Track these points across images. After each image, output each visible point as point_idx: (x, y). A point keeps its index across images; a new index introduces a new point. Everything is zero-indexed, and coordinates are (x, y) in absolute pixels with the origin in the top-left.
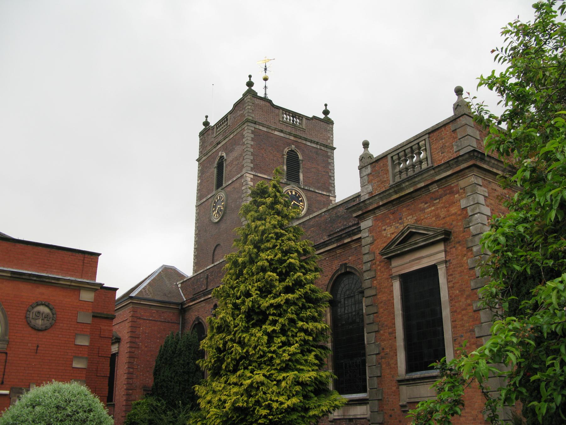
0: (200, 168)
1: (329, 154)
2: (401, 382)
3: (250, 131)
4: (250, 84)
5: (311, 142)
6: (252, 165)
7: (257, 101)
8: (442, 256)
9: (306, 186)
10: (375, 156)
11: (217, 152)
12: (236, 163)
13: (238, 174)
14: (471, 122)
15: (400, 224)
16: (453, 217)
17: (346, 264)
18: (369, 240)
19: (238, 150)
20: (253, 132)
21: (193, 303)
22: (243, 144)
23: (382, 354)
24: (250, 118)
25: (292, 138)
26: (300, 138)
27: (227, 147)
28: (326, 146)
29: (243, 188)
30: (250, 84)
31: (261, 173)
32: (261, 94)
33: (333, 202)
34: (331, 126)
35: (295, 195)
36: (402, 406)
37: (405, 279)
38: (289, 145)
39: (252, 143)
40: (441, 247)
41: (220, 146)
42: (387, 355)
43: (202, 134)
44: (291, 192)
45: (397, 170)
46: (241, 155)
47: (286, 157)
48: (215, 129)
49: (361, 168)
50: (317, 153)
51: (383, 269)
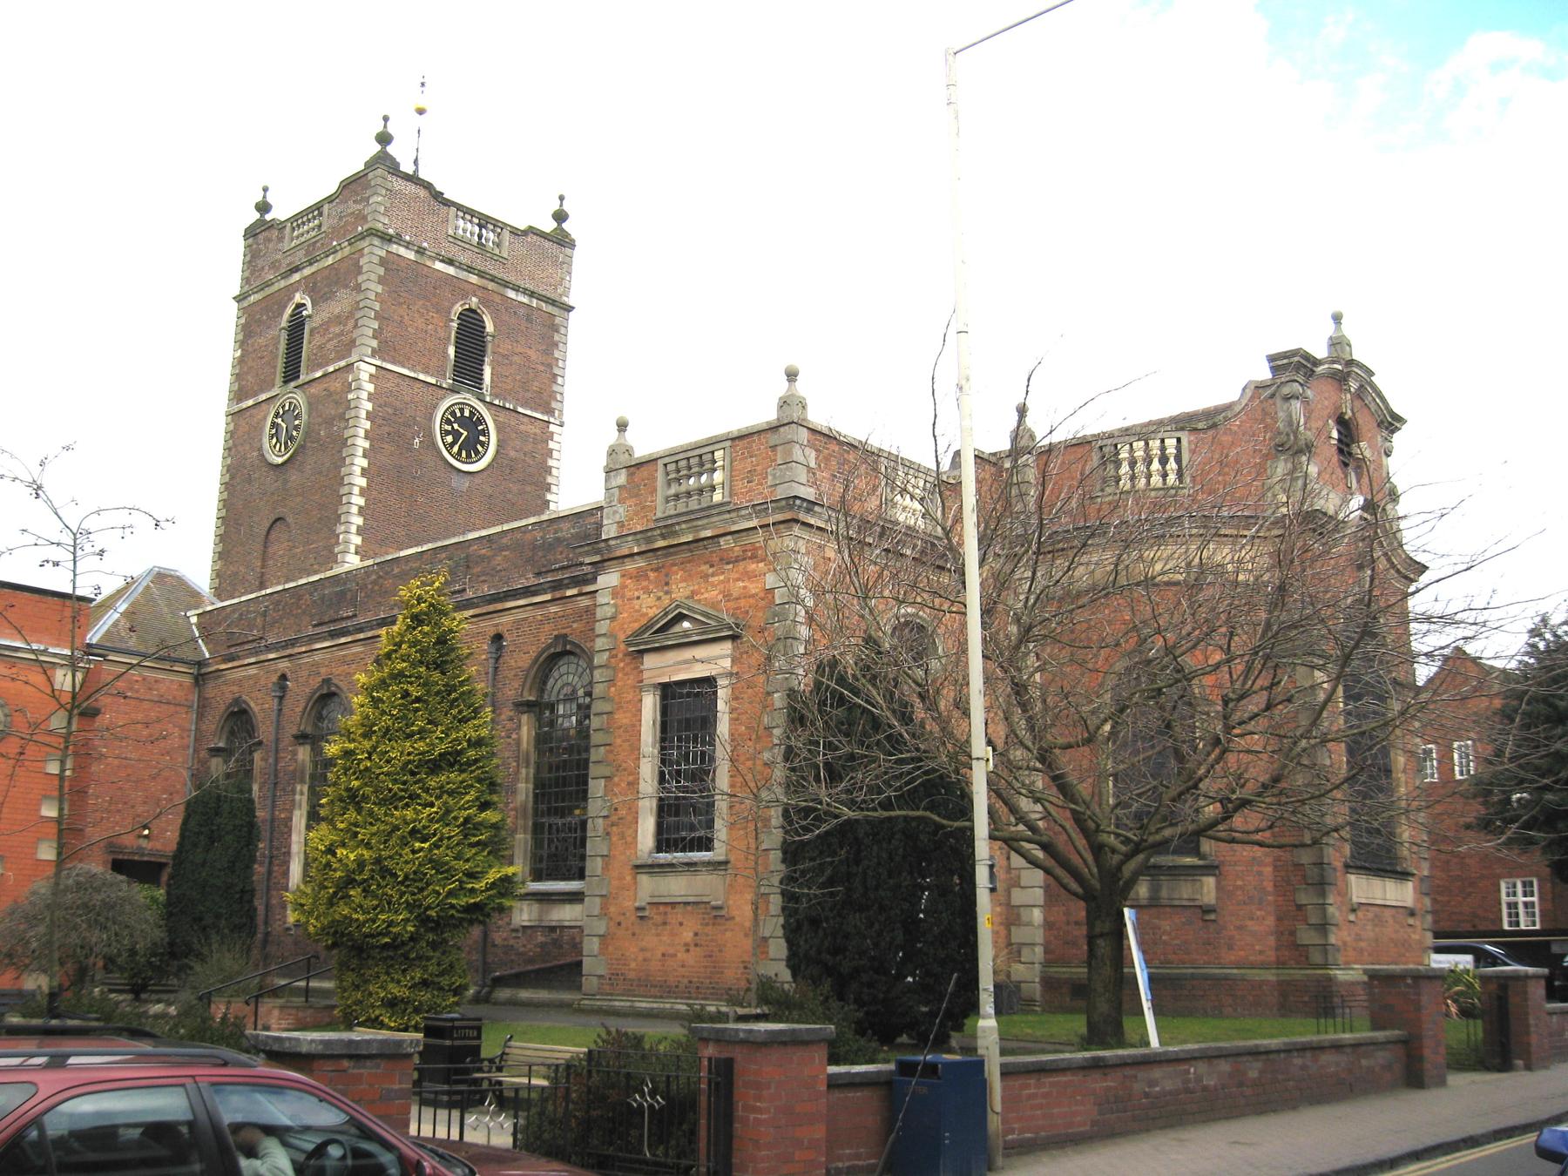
0: (243, 321)
1: (558, 320)
2: (639, 868)
3: (376, 260)
4: (384, 139)
5: (516, 289)
6: (375, 343)
7: (398, 184)
8: (727, 663)
9: (497, 396)
10: (637, 455)
11: (290, 291)
12: (337, 330)
13: (340, 359)
14: (804, 435)
15: (667, 593)
16: (752, 601)
17: (565, 636)
18: (609, 611)
19: (341, 303)
20: (383, 262)
21: (230, 665)
22: (358, 288)
23: (614, 818)
24: (380, 226)
25: (474, 279)
26: (493, 279)
27: (315, 284)
28: (553, 303)
29: (350, 396)
30: (384, 139)
31: (393, 363)
32: (407, 167)
33: (552, 506)
34: (568, 251)
35: (471, 418)
36: (639, 909)
37: (668, 691)
38: (465, 296)
39: (379, 289)
40: (727, 647)
41: (296, 277)
42: (624, 821)
43: (251, 233)
44: (462, 410)
45: (672, 491)
46: (351, 314)
47: (455, 325)
48: (288, 229)
49: (609, 471)
50: (529, 319)
51: (628, 669)
